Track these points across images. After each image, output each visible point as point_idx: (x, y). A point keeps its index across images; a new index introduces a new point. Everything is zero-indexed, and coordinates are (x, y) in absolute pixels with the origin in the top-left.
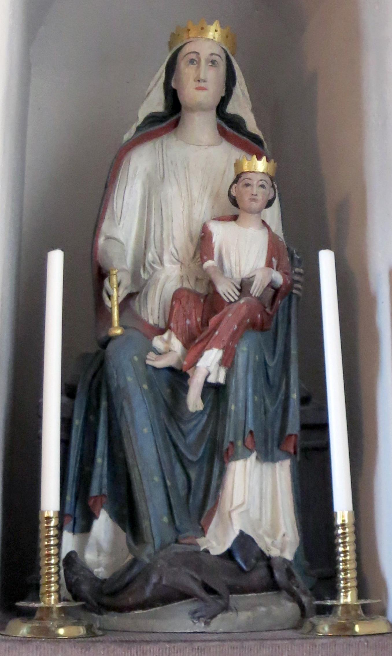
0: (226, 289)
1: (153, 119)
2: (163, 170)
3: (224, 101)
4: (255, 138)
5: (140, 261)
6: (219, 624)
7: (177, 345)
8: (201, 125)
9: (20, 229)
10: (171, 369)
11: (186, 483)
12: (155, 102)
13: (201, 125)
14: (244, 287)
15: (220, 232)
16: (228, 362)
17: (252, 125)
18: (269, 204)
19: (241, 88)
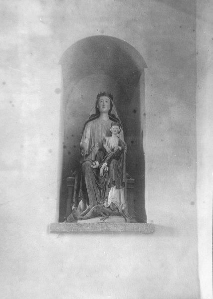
0: (108, 150)
1: (93, 115)
2: (120, 197)
3: (110, 111)
4: (117, 119)
5: (90, 147)
6: (107, 221)
7: (98, 163)
8: (105, 117)
9: (65, 130)
10: (96, 168)
11: (86, 126)
12: (94, 112)
13: (105, 117)
14: (113, 150)
15: (107, 138)
16: (108, 166)
17: (117, 116)
18: (119, 133)
19: (114, 108)
